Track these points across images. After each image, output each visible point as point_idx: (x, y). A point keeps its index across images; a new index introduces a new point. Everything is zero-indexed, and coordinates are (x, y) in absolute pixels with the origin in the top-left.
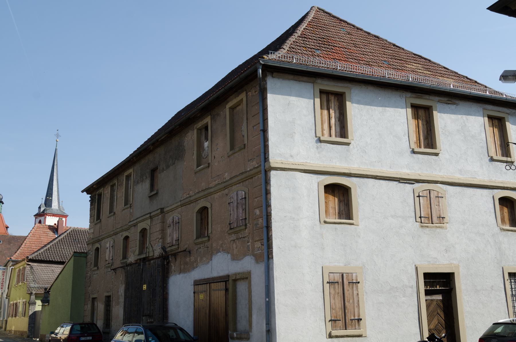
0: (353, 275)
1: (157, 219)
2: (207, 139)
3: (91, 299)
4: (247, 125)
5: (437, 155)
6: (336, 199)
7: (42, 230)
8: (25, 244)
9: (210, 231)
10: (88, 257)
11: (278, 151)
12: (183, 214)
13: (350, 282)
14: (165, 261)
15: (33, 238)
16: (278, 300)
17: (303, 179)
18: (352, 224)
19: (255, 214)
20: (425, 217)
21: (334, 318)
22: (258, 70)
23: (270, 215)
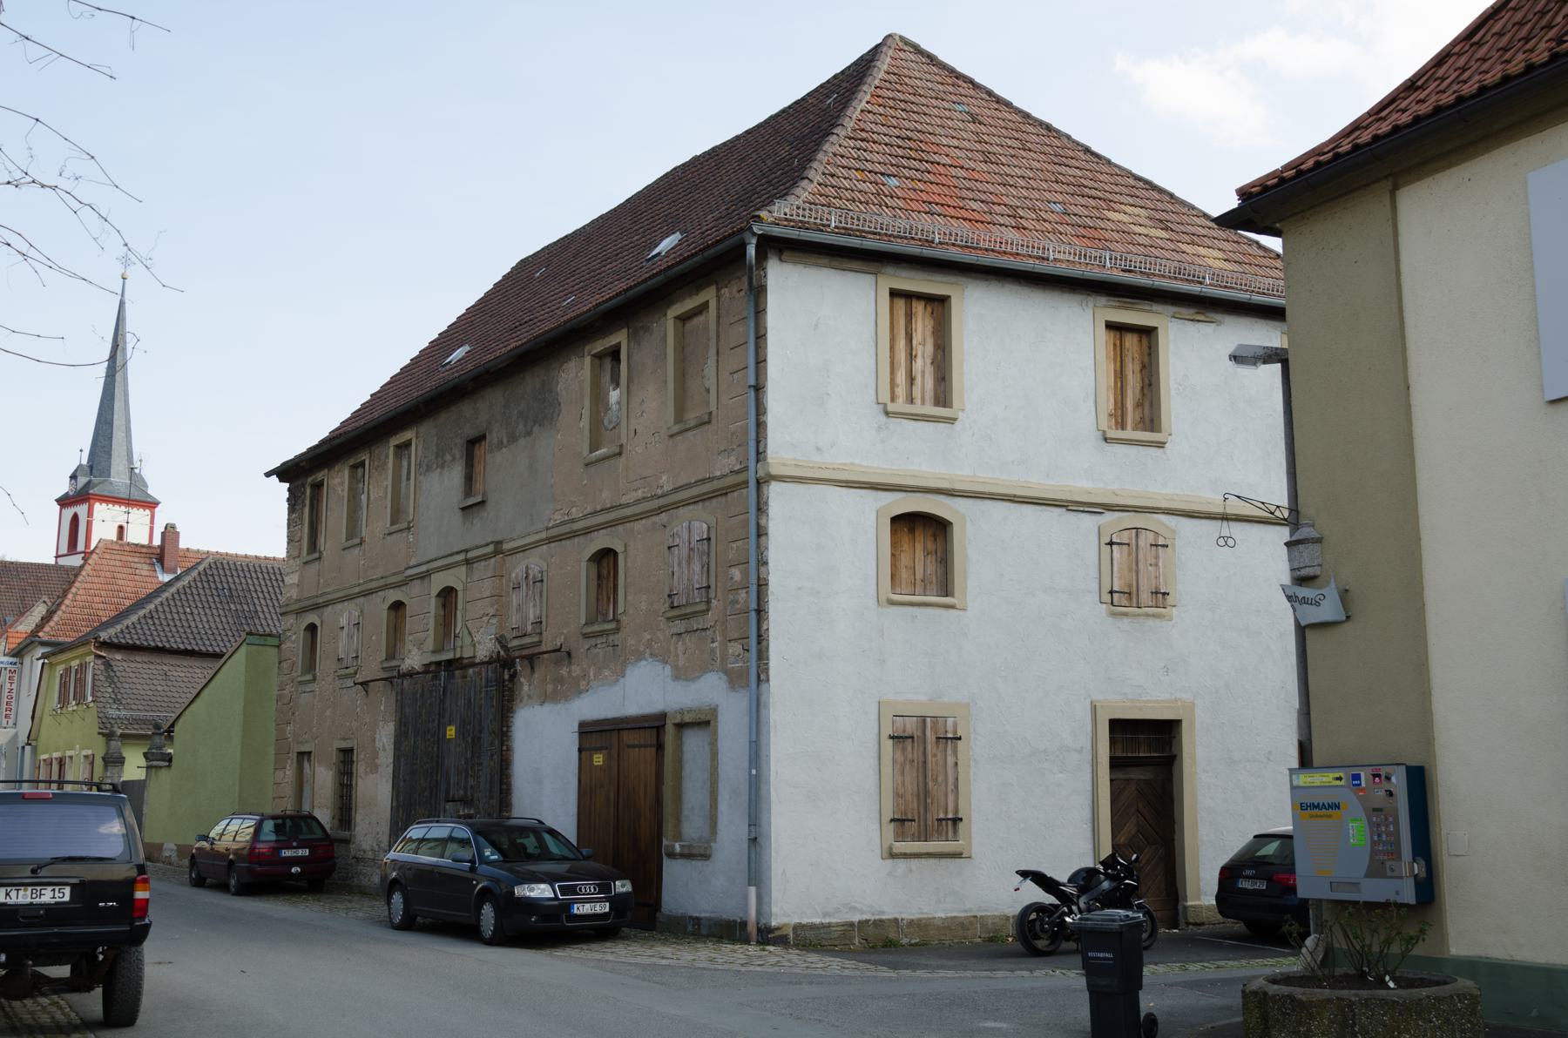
1: (485, 566)
2: (616, 382)
3: (295, 755)
4: (717, 367)
5: (1160, 445)
7: (118, 557)
8: (74, 596)
9: (620, 610)
10: (283, 646)
12: (553, 560)
13: (941, 738)
14: (506, 671)
15: (96, 580)
18: (952, 607)
19: (732, 578)
20: (1121, 592)
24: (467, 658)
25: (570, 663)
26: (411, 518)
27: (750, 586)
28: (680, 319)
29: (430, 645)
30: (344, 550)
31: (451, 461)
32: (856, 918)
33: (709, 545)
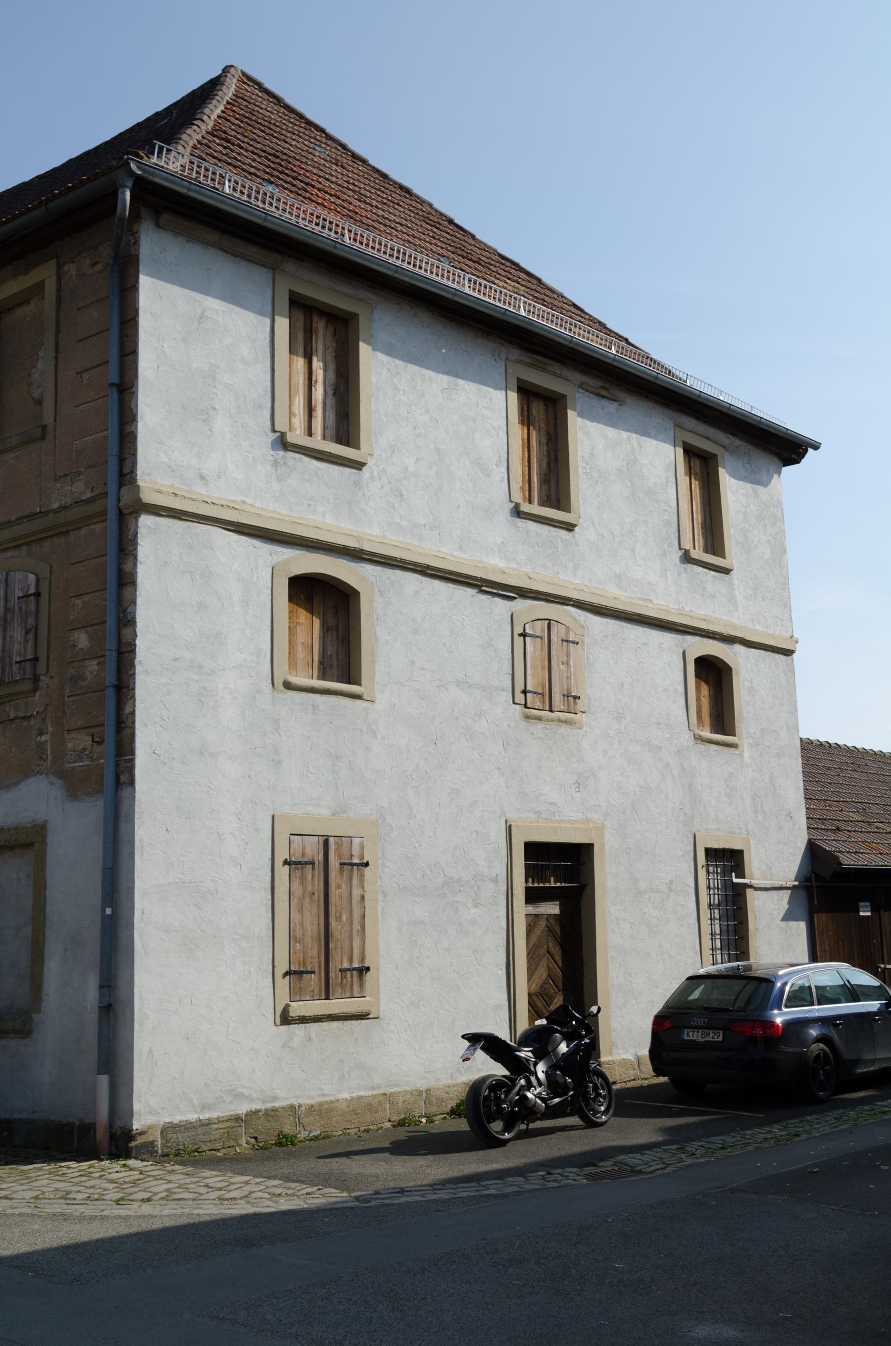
0: (353, 843)
5: (569, 527)
6: (317, 622)
11: (163, 458)
16: (143, 913)
17: (233, 552)
18: (357, 697)
19: (74, 646)
20: (535, 693)
21: (297, 966)
22: (120, 191)
23: (130, 649)
27: (107, 653)
32: (242, 1109)
33: (38, 604)
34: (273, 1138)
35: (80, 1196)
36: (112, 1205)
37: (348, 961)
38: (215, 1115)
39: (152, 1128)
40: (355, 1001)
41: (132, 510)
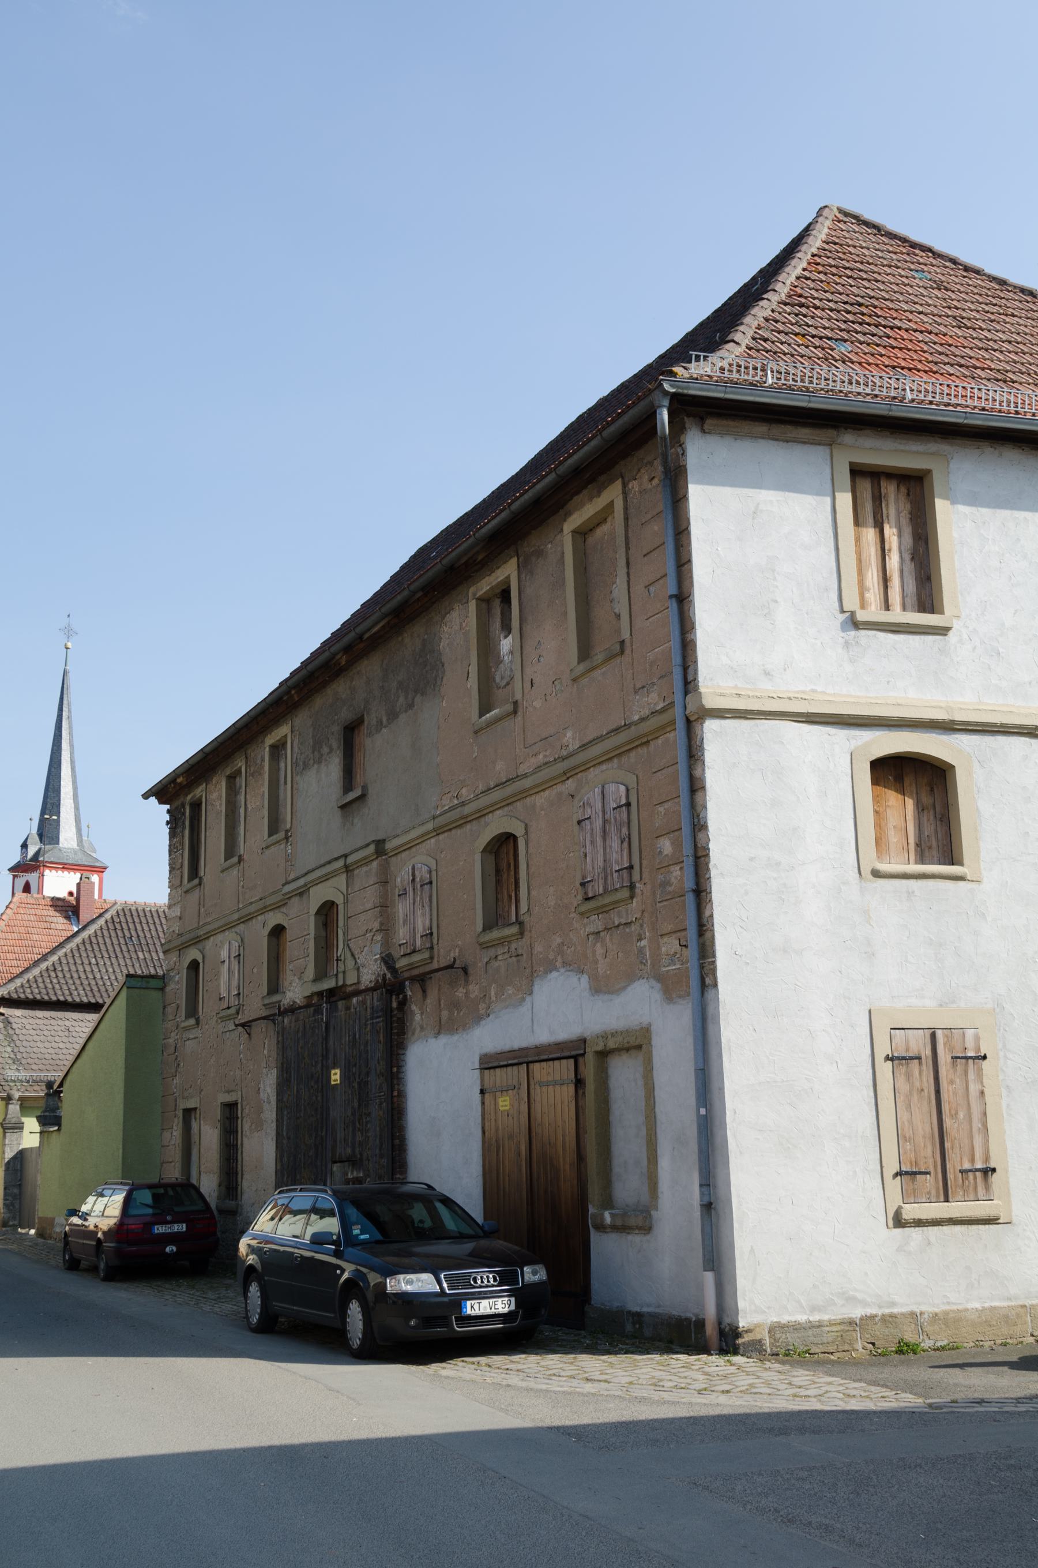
1: (366, 872)
2: (507, 629)
3: (181, 1111)
4: (628, 582)
6: (910, 803)
7: (33, 911)
10: (168, 989)
12: (442, 856)
14: (394, 997)
16: (735, 1113)
18: (961, 878)
23: (704, 853)
24: (351, 985)
25: (467, 982)
26: (288, 826)
28: (577, 533)
29: (310, 973)
30: (222, 871)
31: (328, 753)
32: (857, 1313)
34: (892, 1345)
35: (670, 1384)
36: (694, 1394)
37: (969, 1161)
38: (826, 1317)
39: (759, 1327)
40: (980, 1205)
41: (697, 717)
